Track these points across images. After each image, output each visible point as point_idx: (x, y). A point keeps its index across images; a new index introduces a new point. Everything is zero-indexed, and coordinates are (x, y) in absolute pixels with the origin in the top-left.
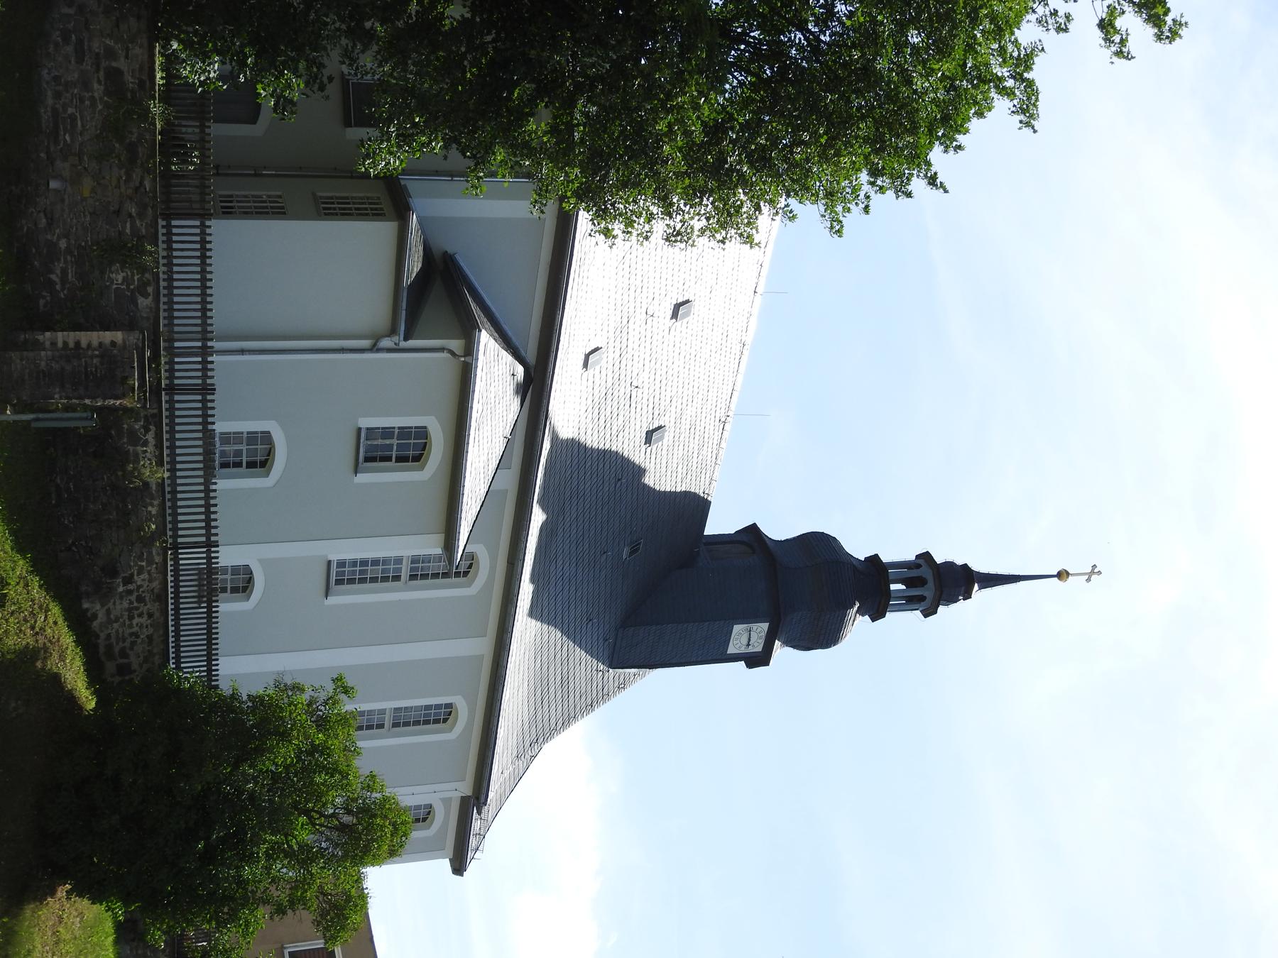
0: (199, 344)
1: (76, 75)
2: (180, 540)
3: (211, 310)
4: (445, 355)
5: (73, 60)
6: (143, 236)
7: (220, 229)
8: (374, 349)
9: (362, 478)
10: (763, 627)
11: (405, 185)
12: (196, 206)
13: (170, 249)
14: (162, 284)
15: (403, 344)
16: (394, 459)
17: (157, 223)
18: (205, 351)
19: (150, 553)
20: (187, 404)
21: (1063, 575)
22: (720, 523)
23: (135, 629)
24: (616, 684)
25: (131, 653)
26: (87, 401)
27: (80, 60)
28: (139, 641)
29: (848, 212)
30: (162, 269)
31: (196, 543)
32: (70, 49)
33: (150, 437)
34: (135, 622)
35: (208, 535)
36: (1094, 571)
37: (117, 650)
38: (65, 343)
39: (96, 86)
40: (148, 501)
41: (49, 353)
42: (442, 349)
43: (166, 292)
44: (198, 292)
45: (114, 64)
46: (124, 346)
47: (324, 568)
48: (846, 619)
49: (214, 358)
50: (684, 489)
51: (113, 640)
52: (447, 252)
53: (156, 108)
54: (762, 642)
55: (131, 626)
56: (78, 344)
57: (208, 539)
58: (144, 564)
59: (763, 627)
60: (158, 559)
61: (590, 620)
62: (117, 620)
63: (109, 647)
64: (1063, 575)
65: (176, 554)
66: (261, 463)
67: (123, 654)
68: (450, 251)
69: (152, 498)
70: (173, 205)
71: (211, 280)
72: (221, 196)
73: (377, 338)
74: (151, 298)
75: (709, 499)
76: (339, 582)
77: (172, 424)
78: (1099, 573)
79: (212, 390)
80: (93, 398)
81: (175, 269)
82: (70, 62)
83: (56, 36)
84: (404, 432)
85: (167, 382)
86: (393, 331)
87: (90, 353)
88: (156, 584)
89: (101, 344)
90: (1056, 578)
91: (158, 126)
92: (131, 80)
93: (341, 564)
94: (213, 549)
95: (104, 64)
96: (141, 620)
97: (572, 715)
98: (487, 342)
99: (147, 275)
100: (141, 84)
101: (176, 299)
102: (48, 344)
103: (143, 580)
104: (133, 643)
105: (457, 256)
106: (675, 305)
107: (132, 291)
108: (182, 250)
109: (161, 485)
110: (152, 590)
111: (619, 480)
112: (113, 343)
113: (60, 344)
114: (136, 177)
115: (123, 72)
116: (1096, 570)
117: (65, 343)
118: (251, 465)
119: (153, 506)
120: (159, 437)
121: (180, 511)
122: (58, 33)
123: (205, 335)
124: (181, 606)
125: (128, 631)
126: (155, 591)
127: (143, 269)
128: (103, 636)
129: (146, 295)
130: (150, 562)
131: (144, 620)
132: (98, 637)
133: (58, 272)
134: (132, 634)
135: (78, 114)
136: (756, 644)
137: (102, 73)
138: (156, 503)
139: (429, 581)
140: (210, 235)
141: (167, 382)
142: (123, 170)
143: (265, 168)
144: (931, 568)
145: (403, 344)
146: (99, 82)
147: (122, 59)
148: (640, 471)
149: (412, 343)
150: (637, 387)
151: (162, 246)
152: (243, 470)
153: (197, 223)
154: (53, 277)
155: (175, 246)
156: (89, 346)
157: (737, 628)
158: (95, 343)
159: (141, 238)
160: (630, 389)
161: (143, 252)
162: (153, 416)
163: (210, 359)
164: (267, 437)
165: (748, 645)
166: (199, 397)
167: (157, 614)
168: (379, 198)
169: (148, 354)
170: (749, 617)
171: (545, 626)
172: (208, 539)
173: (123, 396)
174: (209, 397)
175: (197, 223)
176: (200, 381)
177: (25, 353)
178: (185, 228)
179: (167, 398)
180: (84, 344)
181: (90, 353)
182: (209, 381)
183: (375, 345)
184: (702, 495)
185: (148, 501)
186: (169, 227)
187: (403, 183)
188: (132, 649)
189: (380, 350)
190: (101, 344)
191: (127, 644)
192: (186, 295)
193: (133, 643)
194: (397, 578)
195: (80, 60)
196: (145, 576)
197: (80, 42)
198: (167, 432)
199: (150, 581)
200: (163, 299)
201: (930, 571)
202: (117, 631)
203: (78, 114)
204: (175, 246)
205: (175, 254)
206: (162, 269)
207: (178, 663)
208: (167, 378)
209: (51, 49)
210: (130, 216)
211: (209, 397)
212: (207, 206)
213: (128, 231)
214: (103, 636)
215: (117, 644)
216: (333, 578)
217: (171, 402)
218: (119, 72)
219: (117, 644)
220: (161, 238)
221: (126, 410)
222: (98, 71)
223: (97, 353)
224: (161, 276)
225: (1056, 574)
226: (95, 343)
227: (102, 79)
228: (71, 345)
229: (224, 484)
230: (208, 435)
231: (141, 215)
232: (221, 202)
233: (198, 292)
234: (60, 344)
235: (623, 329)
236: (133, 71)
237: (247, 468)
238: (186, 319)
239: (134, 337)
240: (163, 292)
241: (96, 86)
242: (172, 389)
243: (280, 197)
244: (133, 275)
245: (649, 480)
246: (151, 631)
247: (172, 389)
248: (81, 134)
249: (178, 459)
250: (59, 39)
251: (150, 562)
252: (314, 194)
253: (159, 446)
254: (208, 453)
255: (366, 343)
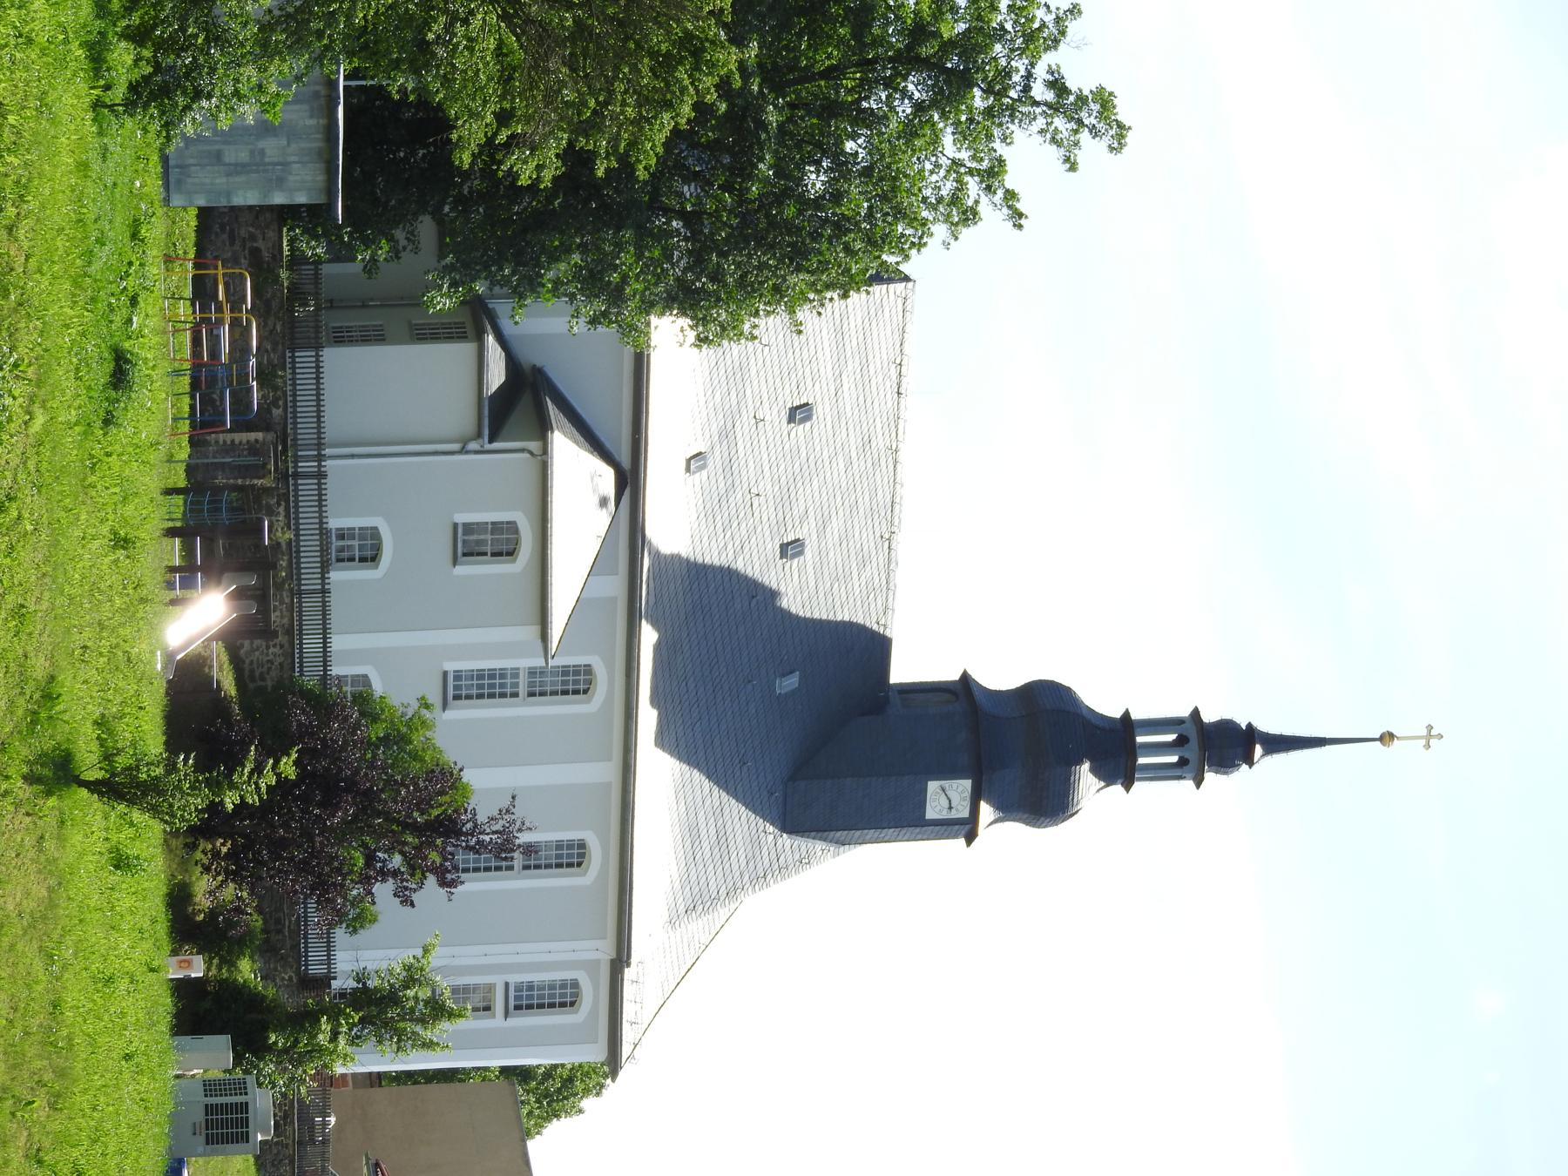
0: (316, 453)
1: (230, 254)
2: (303, 588)
3: (324, 417)
4: (527, 455)
5: (228, 244)
6: (276, 365)
7: (333, 357)
8: (463, 451)
9: (461, 570)
10: (966, 785)
11: (494, 308)
12: (313, 341)
13: (294, 373)
14: (289, 399)
15: (488, 447)
16: (489, 554)
17: (285, 354)
18: (320, 458)
19: (281, 596)
20: (307, 487)
21: (1387, 738)
22: (904, 670)
23: (271, 657)
24: (797, 857)
25: (267, 677)
26: (240, 481)
27: (232, 243)
28: (273, 667)
29: (698, 338)
30: (289, 388)
31: (314, 590)
32: (225, 236)
33: (281, 509)
34: (270, 651)
35: (323, 584)
36: (1430, 736)
37: (257, 674)
38: (225, 442)
39: (243, 261)
40: (280, 556)
41: (215, 448)
42: (522, 450)
43: (291, 404)
44: (314, 403)
45: (255, 245)
46: (264, 443)
47: (442, 675)
48: (1072, 778)
49: (328, 463)
50: (847, 618)
51: (255, 666)
52: (535, 365)
53: (284, 274)
54: (967, 804)
55: (267, 655)
56: (233, 441)
57: (323, 587)
58: (277, 603)
59: (966, 785)
60: (287, 600)
61: (744, 763)
62: (258, 649)
63: (252, 671)
64: (1387, 738)
65: (300, 598)
66: (371, 557)
67: (263, 679)
68: (539, 364)
69: (283, 554)
70: (298, 341)
71: (323, 395)
72: (334, 328)
73: (465, 443)
74: (281, 409)
75: (888, 633)
76: (457, 697)
77: (297, 502)
78: (1440, 736)
79: (325, 476)
80: (244, 478)
81: (298, 387)
82: (225, 245)
83: (216, 228)
84: (496, 527)
85: (293, 470)
86: (479, 435)
87: (241, 447)
88: (286, 621)
89: (248, 442)
90: (1378, 743)
91: (285, 284)
92: (267, 255)
93: (458, 676)
94: (327, 595)
95: (248, 245)
96: (275, 650)
97: (739, 884)
98: (566, 450)
99: (278, 393)
100: (274, 257)
101: (299, 409)
102: (213, 442)
103: (277, 617)
104: (269, 669)
105: (544, 369)
106: (791, 409)
107: (268, 404)
108: (303, 373)
109: (289, 542)
110: (283, 625)
111: (753, 597)
112: (257, 441)
113: (221, 442)
114: (270, 323)
115: (261, 250)
116: (1433, 733)
117: (225, 442)
118: (363, 560)
119: (283, 561)
120: (287, 509)
121: (297, 365)
122: (217, 226)
123: (320, 446)
124: (304, 641)
125: (265, 659)
126: (286, 626)
127: (275, 388)
128: (247, 661)
129: (278, 407)
130: (282, 602)
131: (277, 650)
132: (244, 662)
133: (218, 392)
134: (268, 661)
135: (231, 281)
136: (960, 808)
137: (247, 252)
138: (285, 558)
139: (548, 698)
140: (322, 362)
141: (293, 470)
142: (262, 319)
143: (372, 300)
144: (1196, 725)
145: (488, 447)
146: (245, 258)
147: (261, 241)
148: (773, 595)
149: (496, 445)
150: (758, 495)
151: (289, 371)
152: (356, 563)
153: (314, 354)
154: (215, 396)
155: (298, 371)
156: (240, 443)
157: (933, 786)
158: (244, 441)
159: (274, 366)
160: (749, 497)
161: (276, 376)
162: (284, 494)
163: (323, 463)
164: (374, 533)
165: (950, 808)
166: (316, 481)
167: (287, 645)
168: (464, 323)
169: (280, 448)
170: (948, 771)
171: (685, 767)
172: (323, 587)
173: (263, 477)
174: (323, 481)
175: (314, 354)
176: (316, 469)
177: (199, 448)
178: (304, 357)
179: (293, 482)
180: (237, 442)
181: (241, 447)
182: (323, 469)
183: (463, 447)
184: (875, 627)
185: (280, 556)
186: (293, 357)
187: (490, 306)
188: (268, 673)
189: (467, 452)
190: (248, 442)
191: (265, 669)
192: (305, 406)
193: (269, 669)
194: (515, 695)
195: (232, 243)
196: (278, 613)
197: (232, 231)
198: (292, 485)
199: (282, 617)
200: (290, 410)
201: (1194, 727)
202: (258, 659)
203: (231, 281)
204: (298, 371)
205: (298, 376)
206: (289, 388)
207: (301, 671)
208: (292, 467)
209: (213, 237)
210: (267, 351)
211: (323, 481)
212: (320, 341)
213: (265, 362)
214: (247, 661)
215: (258, 668)
216: (451, 692)
217: (296, 485)
218: (258, 250)
219: (258, 668)
220: (288, 366)
221: (265, 490)
222: (244, 250)
223: (246, 447)
224: (288, 393)
225: (1378, 736)
226: (244, 441)
227: (247, 256)
228: (229, 443)
229: (337, 576)
230: (324, 532)
231: (274, 350)
232: (334, 332)
233: (314, 403)
234: (221, 442)
235: (726, 434)
236: (268, 249)
237: (359, 561)
238: (305, 431)
239: (270, 436)
240: (290, 404)
241: (243, 261)
242: (296, 475)
243: (381, 325)
244: (269, 393)
245: (784, 603)
246: (282, 659)
247: (296, 475)
248: (233, 295)
249: (301, 527)
250: (218, 230)
251: (282, 602)
252: (410, 323)
253: (287, 516)
254: (324, 549)
255: (456, 447)
